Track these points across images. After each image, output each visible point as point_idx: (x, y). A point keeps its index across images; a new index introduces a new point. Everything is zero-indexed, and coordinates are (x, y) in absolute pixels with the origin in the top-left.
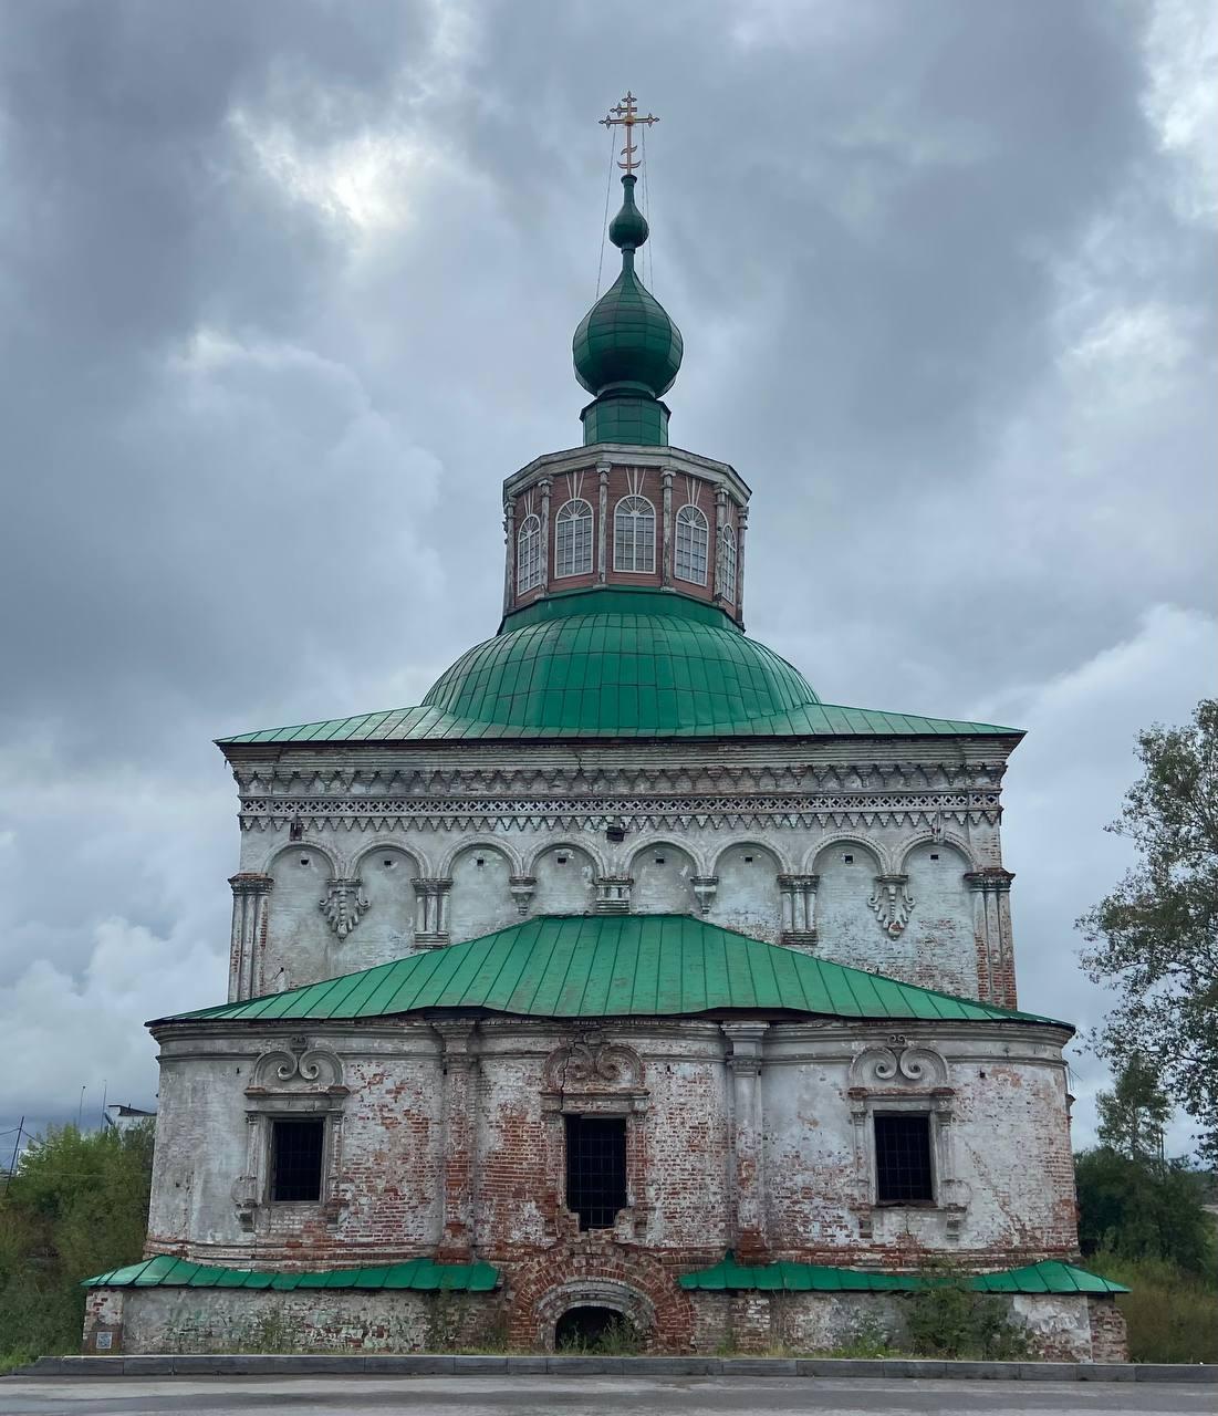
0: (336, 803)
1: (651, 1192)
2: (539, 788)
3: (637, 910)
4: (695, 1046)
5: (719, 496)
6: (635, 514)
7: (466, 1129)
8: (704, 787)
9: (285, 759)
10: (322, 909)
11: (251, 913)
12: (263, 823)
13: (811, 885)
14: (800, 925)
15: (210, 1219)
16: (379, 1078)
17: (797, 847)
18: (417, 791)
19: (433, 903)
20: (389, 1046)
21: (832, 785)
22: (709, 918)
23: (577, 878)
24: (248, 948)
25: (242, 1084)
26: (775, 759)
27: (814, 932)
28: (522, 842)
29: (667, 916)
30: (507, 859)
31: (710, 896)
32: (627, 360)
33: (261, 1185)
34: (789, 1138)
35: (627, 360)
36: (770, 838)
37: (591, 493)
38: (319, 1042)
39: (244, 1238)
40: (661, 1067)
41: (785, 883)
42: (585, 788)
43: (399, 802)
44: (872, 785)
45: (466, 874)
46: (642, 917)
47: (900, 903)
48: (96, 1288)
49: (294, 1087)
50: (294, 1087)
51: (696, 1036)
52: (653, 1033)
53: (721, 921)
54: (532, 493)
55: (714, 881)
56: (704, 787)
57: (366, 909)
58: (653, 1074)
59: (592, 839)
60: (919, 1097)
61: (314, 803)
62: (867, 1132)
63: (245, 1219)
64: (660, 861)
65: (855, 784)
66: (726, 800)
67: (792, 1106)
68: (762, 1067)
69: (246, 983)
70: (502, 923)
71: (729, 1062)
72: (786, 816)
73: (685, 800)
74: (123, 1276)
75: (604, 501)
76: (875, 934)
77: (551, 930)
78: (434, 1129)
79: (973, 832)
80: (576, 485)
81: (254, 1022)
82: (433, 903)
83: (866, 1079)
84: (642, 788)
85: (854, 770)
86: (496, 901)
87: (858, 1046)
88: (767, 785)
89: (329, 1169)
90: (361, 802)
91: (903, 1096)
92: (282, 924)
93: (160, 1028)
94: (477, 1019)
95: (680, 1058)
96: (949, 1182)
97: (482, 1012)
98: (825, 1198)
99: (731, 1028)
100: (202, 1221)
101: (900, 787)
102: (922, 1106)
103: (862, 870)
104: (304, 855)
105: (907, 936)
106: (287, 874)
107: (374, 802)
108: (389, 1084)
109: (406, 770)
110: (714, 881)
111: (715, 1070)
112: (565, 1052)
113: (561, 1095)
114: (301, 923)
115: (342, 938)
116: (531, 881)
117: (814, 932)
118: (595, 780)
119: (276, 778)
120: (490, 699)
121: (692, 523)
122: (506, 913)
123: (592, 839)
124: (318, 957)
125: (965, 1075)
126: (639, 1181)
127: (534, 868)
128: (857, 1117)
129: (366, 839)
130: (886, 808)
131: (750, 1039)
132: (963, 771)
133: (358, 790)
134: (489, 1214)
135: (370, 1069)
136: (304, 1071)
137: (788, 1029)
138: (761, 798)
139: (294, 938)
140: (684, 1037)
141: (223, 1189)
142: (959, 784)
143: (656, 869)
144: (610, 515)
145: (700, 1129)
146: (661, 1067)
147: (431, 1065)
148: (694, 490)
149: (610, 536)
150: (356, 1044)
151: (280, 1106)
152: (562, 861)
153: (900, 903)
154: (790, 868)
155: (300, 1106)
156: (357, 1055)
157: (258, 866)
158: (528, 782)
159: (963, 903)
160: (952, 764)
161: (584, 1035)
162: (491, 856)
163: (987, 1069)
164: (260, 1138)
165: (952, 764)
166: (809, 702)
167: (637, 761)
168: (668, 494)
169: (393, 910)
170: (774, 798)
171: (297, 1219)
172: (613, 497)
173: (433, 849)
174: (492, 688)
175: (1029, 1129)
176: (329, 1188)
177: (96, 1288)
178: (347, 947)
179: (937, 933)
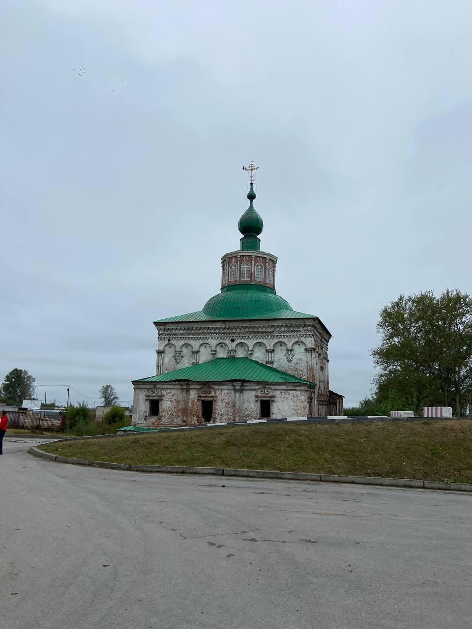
0: (176, 334)
1: (217, 415)
2: (217, 331)
3: (237, 357)
4: (227, 387)
5: (270, 261)
6: (246, 266)
7: (186, 402)
8: (251, 330)
9: (166, 325)
10: (174, 357)
11: (160, 358)
12: (162, 339)
13: (273, 351)
14: (270, 360)
15: (139, 419)
16: (169, 393)
17: (269, 343)
18: (193, 332)
19: (196, 355)
20: (171, 387)
21: (278, 329)
22: (252, 358)
23: (225, 350)
24: (160, 365)
25: (145, 394)
26: (265, 324)
27: (273, 362)
28: (213, 342)
29: (243, 358)
30: (211, 346)
31: (252, 354)
32: (251, 228)
33: (148, 413)
34: (246, 405)
35: (251, 228)
36: (264, 341)
37: (236, 262)
38: (158, 386)
39: (145, 422)
40: (220, 391)
41: (267, 351)
42: (227, 331)
43: (189, 334)
44: (286, 329)
45: (203, 350)
46: (238, 358)
47: (291, 355)
48: (119, 431)
49: (153, 395)
50: (153, 395)
51: (227, 385)
52: (218, 384)
53: (254, 359)
54: (227, 260)
55: (253, 351)
56: (251, 330)
57: (183, 357)
58: (218, 392)
59: (227, 342)
60: (267, 397)
61: (173, 334)
62: (258, 404)
63: (145, 419)
64: (242, 346)
65: (283, 329)
66: (256, 333)
67: (246, 399)
68: (241, 391)
69: (159, 372)
70: (210, 359)
71: (235, 390)
72: (268, 336)
73: (247, 333)
74: (124, 429)
75: (239, 264)
76: (286, 361)
77: (218, 360)
78: (181, 403)
79: (307, 339)
80: (233, 260)
81: (146, 382)
82: (196, 355)
83: (259, 394)
84: (238, 330)
85: (282, 326)
86: (208, 355)
87: (257, 387)
88: (264, 329)
89: (160, 410)
90: (181, 334)
91: (265, 397)
92: (166, 360)
93: (134, 383)
94: (187, 382)
95: (224, 389)
96: (272, 414)
97: (187, 381)
98: (251, 417)
99: (235, 383)
100: (138, 419)
101: (292, 330)
102: (269, 399)
103: (283, 348)
104: (171, 346)
105: (292, 362)
106: (167, 350)
107: (184, 334)
108: (171, 394)
109: (190, 327)
110: (253, 351)
111: (232, 392)
112: (201, 388)
113: (200, 396)
114: (170, 360)
115: (178, 363)
116: (215, 351)
117: (273, 362)
118: (228, 329)
119: (165, 329)
120: (211, 310)
121: (260, 267)
122: (210, 358)
123: (227, 342)
124: (173, 367)
125: (278, 392)
126: (215, 413)
127: (216, 348)
128: (257, 401)
129: (182, 342)
130: (289, 334)
131: (238, 385)
132: (305, 326)
133: (181, 332)
134: (189, 419)
135: (168, 391)
136: (155, 391)
137: (245, 384)
138: (263, 332)
139: (169, 362)
140: (225, 385)
141: (142, 413)
142: (304, 329)
143: (241, 348)
144: (240, 267)
145: (228, 403)
146: (220, 391)
147: (180, 390)
148: (260, 260)
149: (240, 272)
150: (165, 386)
151: (151, 398)
152: (222, 346)
153: (291, 355)
154: (268, 348)
155: (155, 398)
156: (165, 388)
157: (161, 348)
158: (215, 330)
159: (305, 355)
160: (303, 324)
161: (206, 385)
162: (207, 346)
163: (282, 391)
164: (148, 403)
165: (303, 324)
166: (286, 307)
167: (237, 325)
168: (253, 261)
169: (188, 357)
170: (266, 332)
171: (154, 419)
172: (240, 263)
173: (195, 344)
174: (212, 308)
175: (291, 403)
176: (160, 414)
177: (119, 431)
178: (179, 365)
179: (299, 361)
